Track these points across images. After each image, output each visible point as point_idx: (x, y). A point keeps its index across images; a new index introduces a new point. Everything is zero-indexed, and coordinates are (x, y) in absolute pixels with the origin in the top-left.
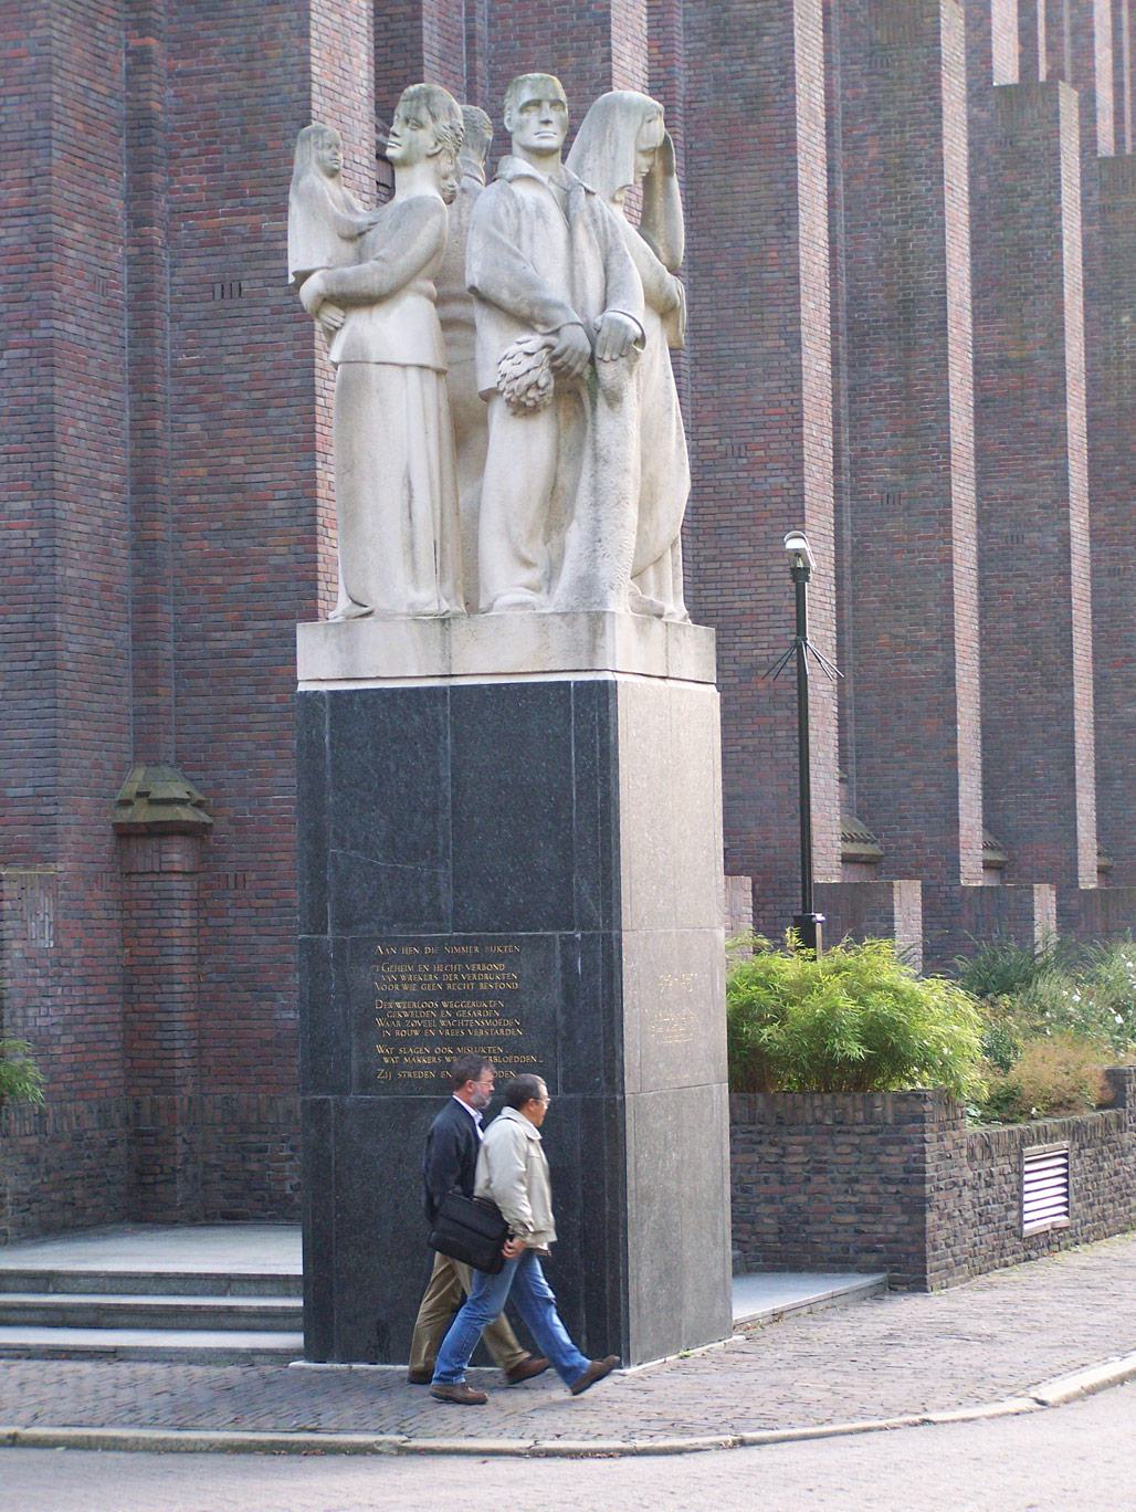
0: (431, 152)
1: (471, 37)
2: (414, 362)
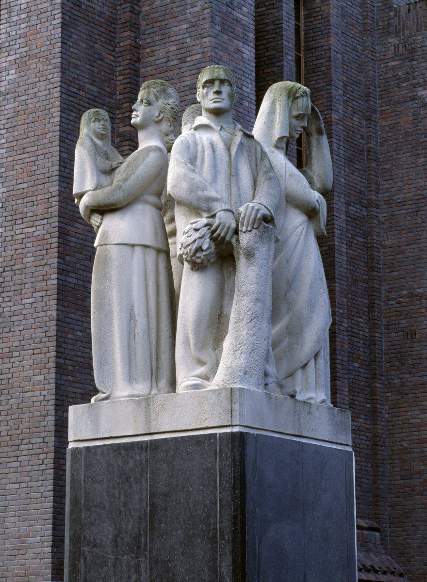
0: (157, 119)
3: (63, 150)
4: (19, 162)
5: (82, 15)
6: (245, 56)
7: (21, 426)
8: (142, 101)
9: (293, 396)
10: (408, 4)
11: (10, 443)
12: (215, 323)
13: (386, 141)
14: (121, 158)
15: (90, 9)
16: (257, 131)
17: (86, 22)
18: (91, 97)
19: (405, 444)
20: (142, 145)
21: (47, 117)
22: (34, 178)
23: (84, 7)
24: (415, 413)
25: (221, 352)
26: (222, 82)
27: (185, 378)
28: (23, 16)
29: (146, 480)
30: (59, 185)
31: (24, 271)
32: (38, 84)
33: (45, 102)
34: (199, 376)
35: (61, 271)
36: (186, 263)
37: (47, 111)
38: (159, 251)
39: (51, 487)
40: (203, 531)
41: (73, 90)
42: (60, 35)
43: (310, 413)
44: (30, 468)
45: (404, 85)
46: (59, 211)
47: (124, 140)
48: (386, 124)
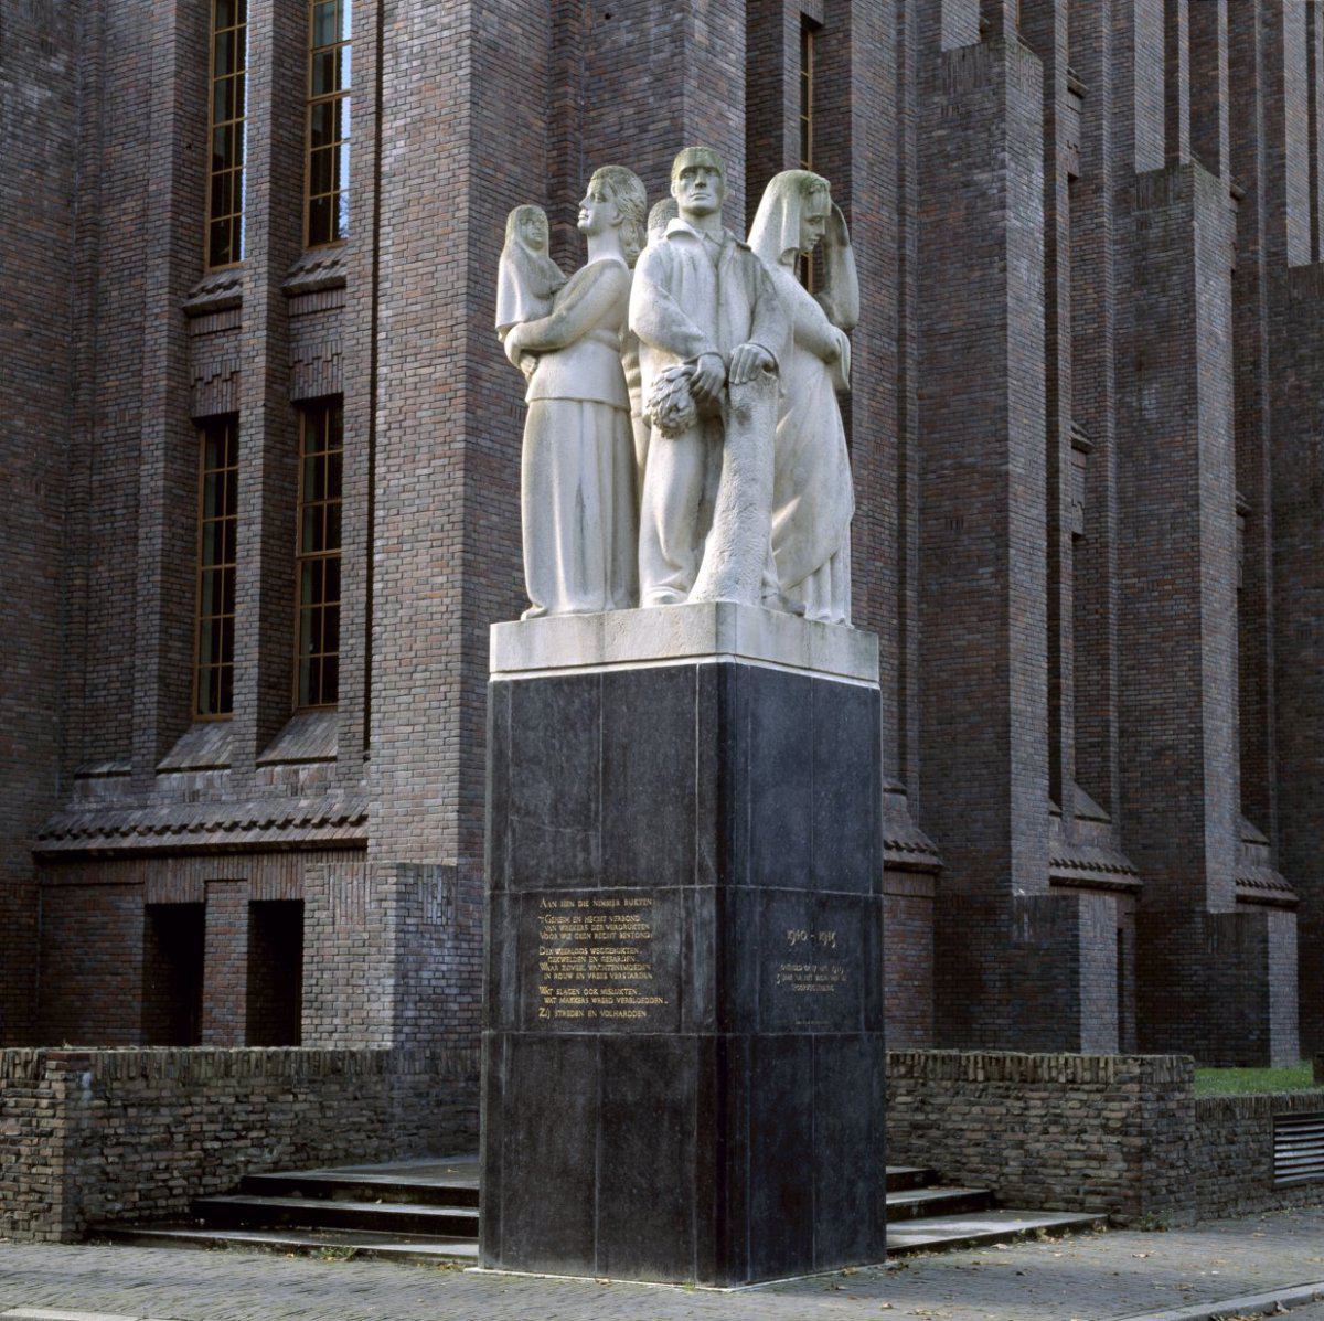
1: (902, 260)
2: (588, 397)
3: (473, 257)
4: (410, 274)
5: (500, 63)
6: (731, 123)
7: (415, 647)
8: (593, 195)
9: (800, 615)
10: (963, 48)
11: (399, 670)
12: (698, 513)
13: (928, 245)
14: (563, 275)
15: (510, 54)
16: (755, 241)
17: (507, 73)
18: (512, 181)
19: (944, 676)
20: (595, 259)
21: (451, 209)
22: (432, 296)
23: (502, 51)
24: (960, 632)
25: (702, 553)
26: (708, 170)
27: (650, 593)
28: (415, 63)
29: (598, 726)
30: (467, 307)
31: (418, 429)
32: (437, 163)
33: (447, 188)
34: (670, 585)
35: (471, 431)
36: (654, 427)
37: (450, 201)
38: (616, 409)
39: (456, 732)
40: (677, 797)
41: (487, 170)
42: (468, 92)
43: (823, 637)
44: (426, 705)
45: (955, 165)
46: (467, 345)
47: (568, 248)
48: (928, 220)
